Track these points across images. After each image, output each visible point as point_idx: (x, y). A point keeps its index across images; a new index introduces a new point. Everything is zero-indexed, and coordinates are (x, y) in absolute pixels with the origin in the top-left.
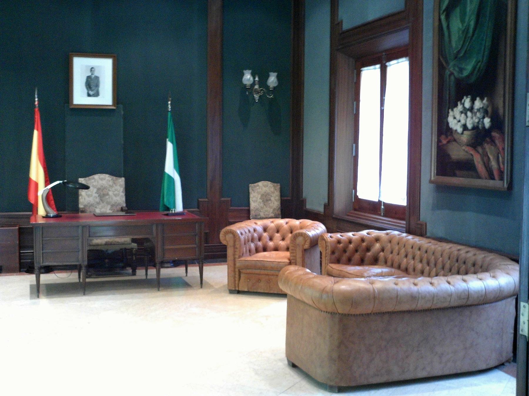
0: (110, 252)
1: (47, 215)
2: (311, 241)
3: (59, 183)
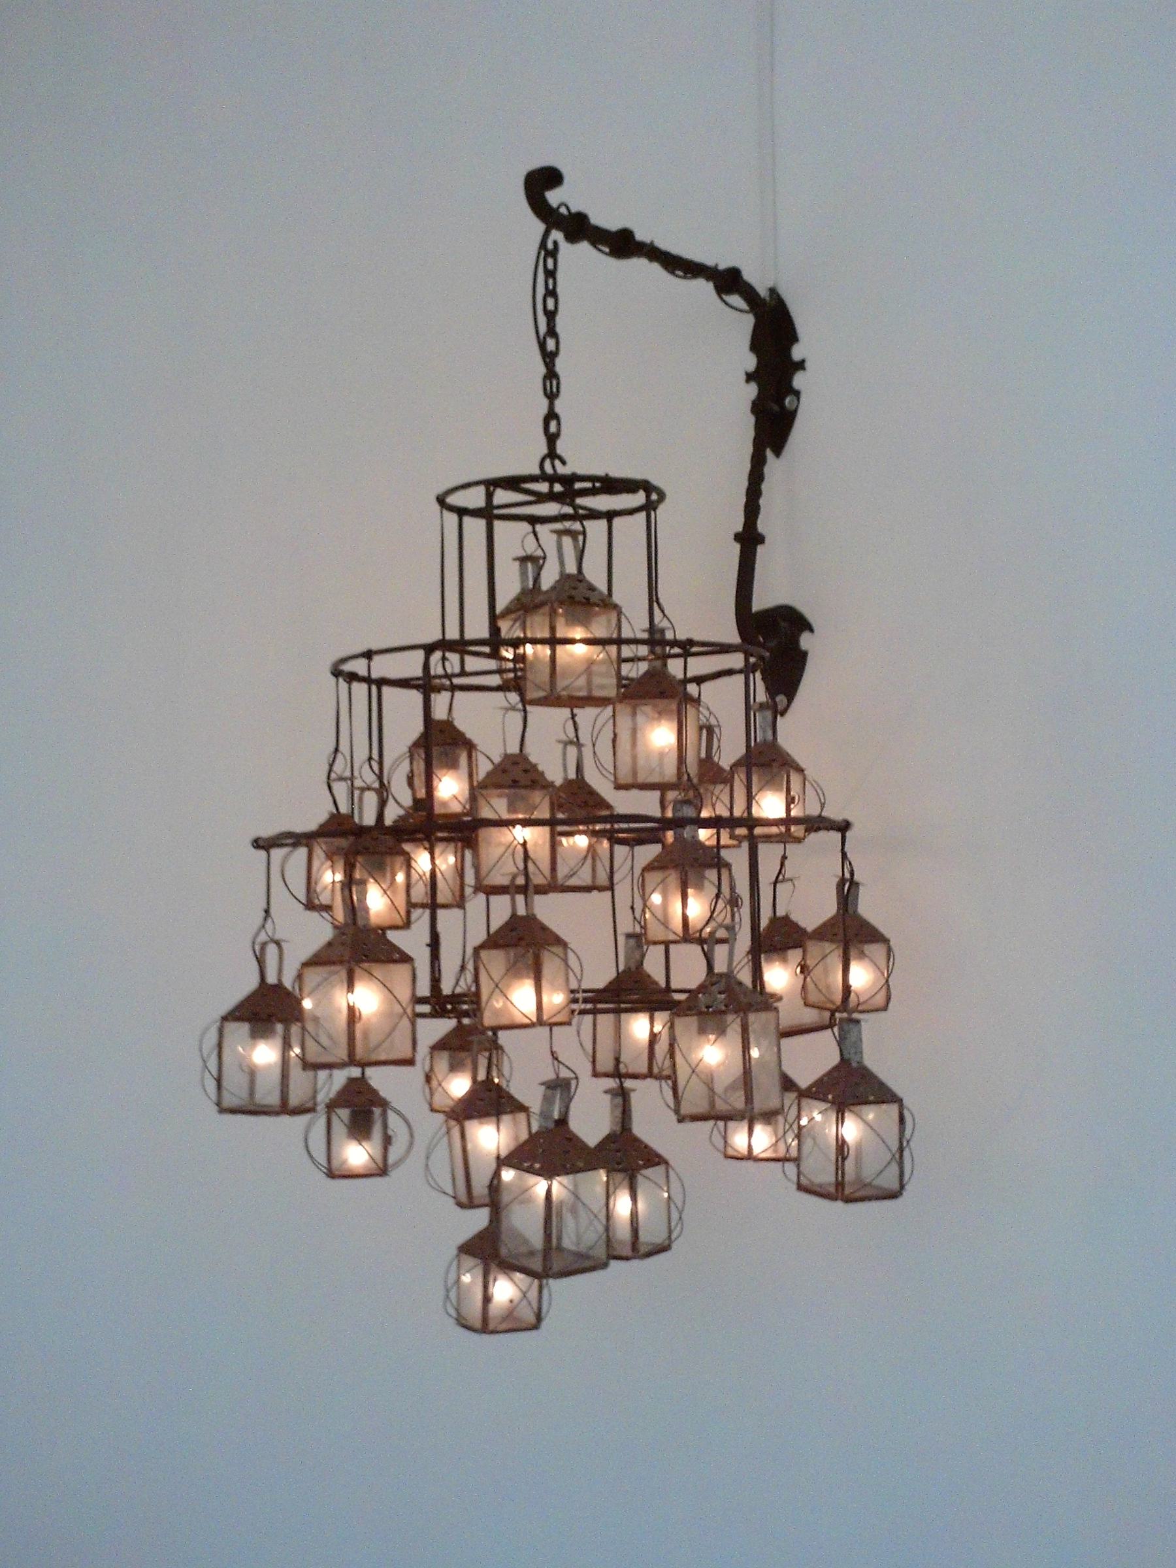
0: (740, 529)
1: (350, 779)
2: (775, 1123)
3: (762, 683)
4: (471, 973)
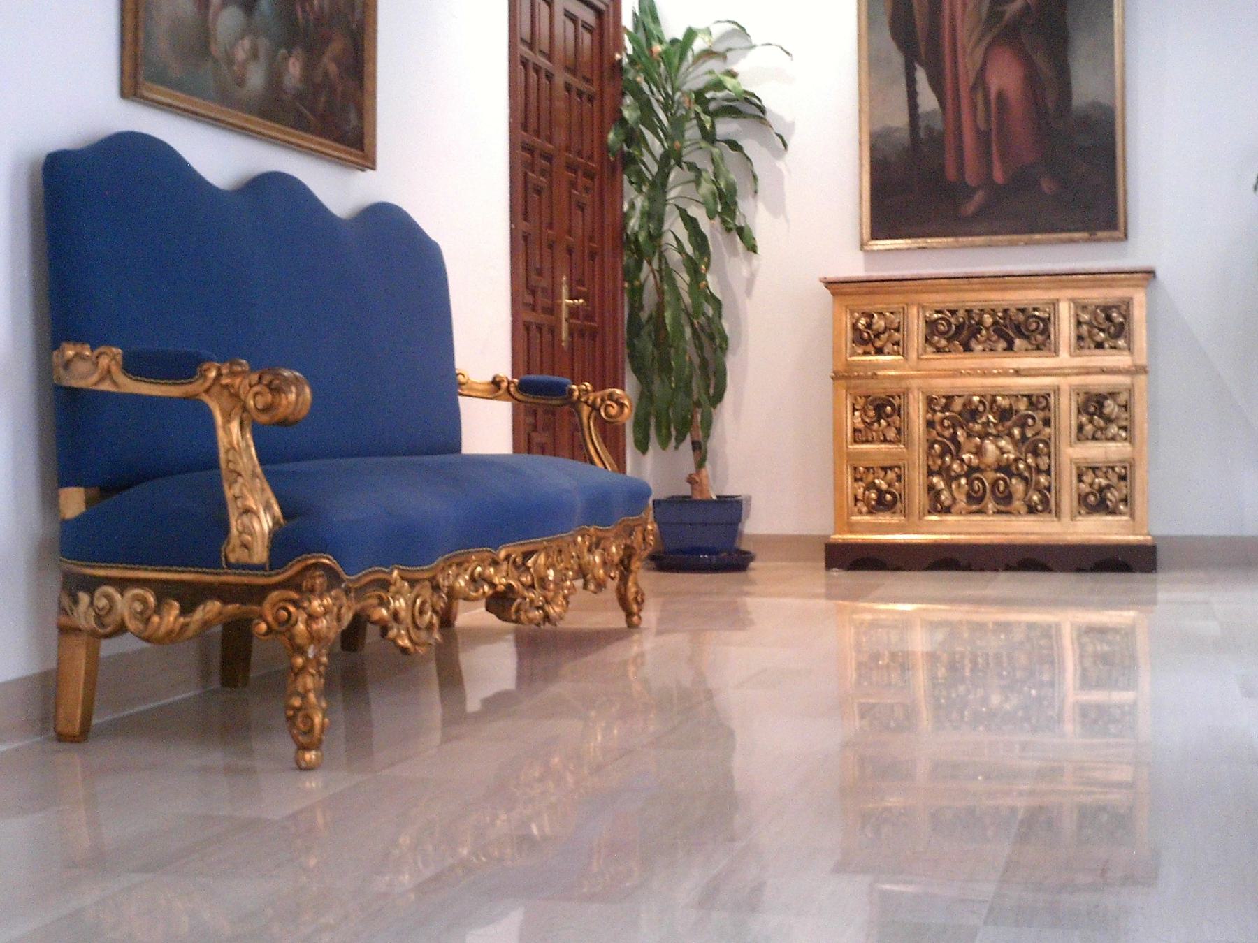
2: (197, 395)
4: (682, 288)
